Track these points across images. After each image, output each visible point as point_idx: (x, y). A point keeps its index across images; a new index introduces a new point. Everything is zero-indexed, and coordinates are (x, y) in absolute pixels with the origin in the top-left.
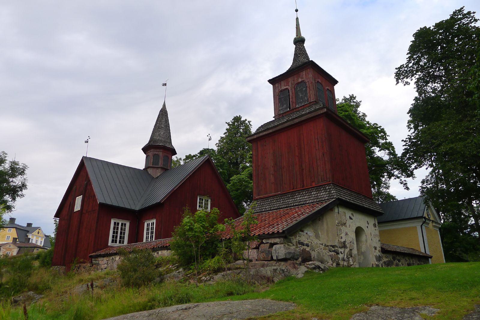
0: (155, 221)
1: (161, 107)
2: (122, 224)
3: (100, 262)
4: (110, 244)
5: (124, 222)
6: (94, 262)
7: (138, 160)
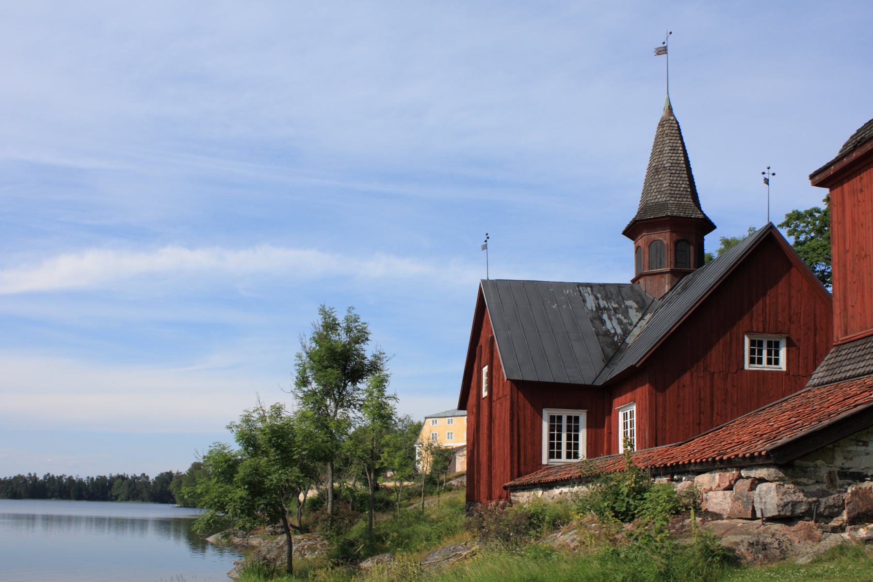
0: (634, 408)
1: (660, 113)
2: (569, 418)
4: (545, 461)
5: (573, 413)
7: (617, 265)
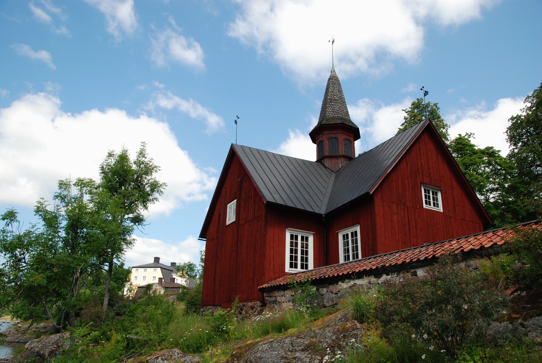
0: (358, 229)
3: (279, 299)
4: (287, 269)
6: (267, 298)
